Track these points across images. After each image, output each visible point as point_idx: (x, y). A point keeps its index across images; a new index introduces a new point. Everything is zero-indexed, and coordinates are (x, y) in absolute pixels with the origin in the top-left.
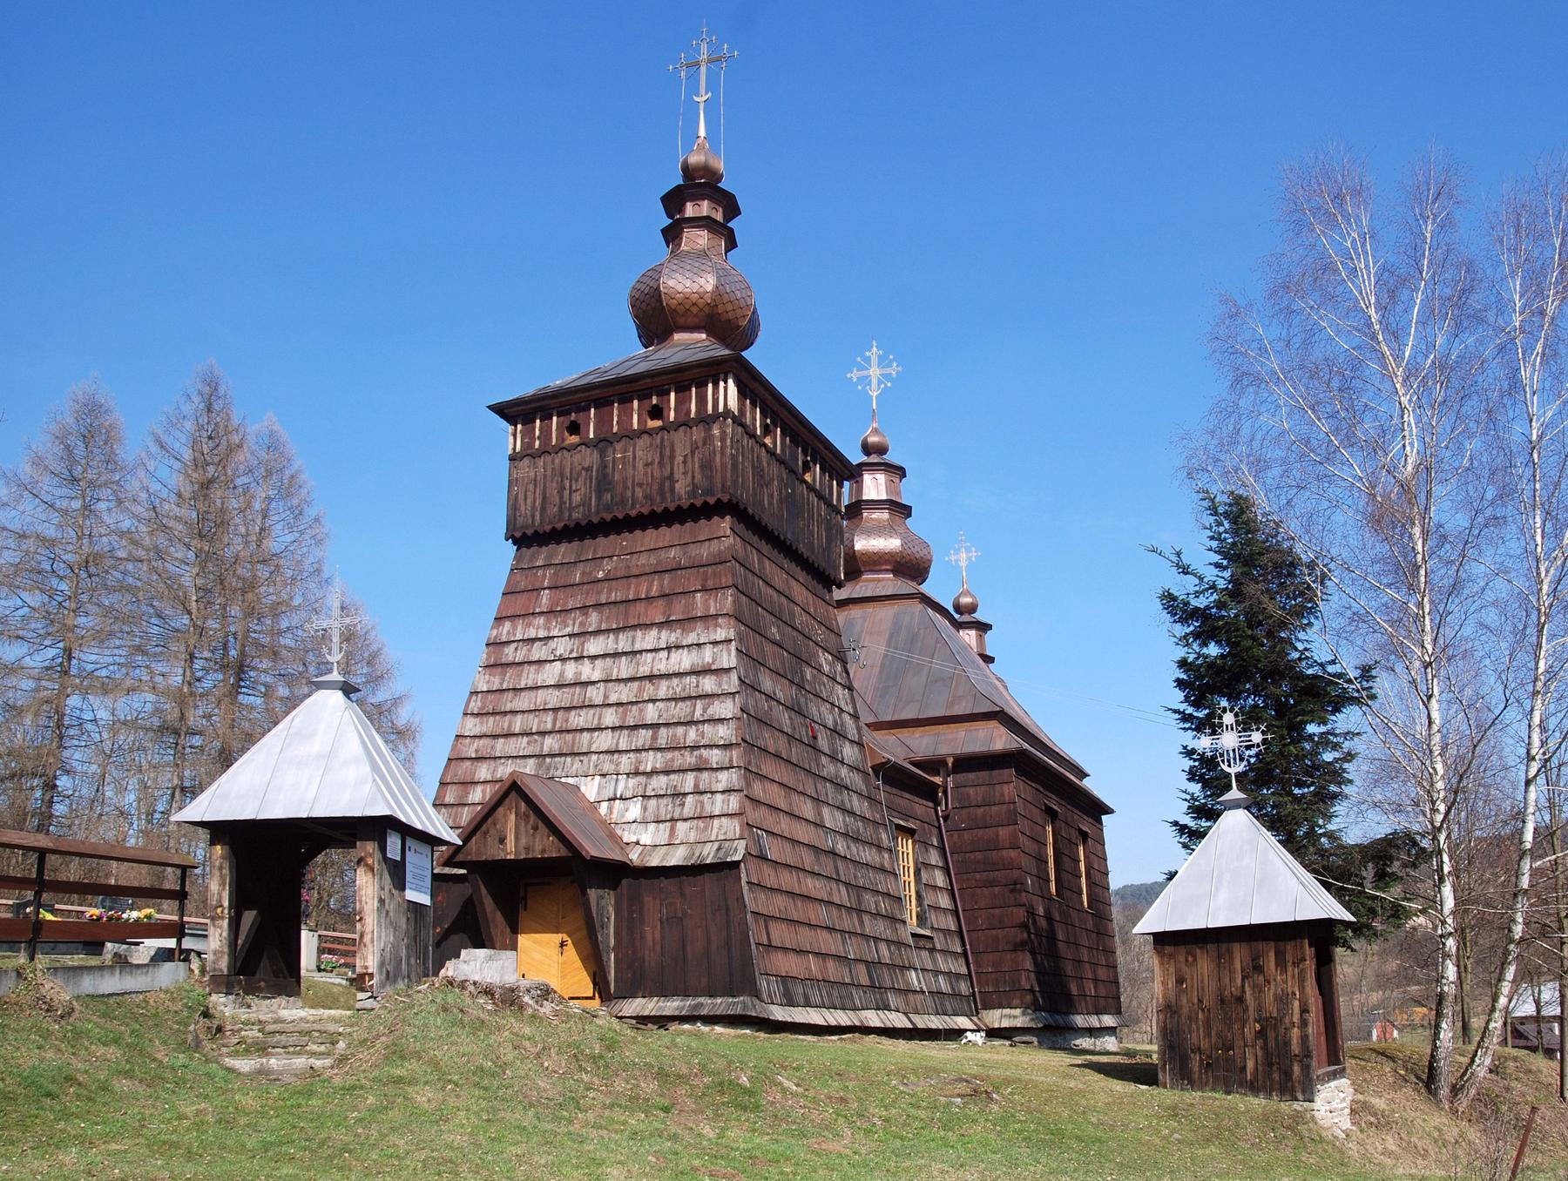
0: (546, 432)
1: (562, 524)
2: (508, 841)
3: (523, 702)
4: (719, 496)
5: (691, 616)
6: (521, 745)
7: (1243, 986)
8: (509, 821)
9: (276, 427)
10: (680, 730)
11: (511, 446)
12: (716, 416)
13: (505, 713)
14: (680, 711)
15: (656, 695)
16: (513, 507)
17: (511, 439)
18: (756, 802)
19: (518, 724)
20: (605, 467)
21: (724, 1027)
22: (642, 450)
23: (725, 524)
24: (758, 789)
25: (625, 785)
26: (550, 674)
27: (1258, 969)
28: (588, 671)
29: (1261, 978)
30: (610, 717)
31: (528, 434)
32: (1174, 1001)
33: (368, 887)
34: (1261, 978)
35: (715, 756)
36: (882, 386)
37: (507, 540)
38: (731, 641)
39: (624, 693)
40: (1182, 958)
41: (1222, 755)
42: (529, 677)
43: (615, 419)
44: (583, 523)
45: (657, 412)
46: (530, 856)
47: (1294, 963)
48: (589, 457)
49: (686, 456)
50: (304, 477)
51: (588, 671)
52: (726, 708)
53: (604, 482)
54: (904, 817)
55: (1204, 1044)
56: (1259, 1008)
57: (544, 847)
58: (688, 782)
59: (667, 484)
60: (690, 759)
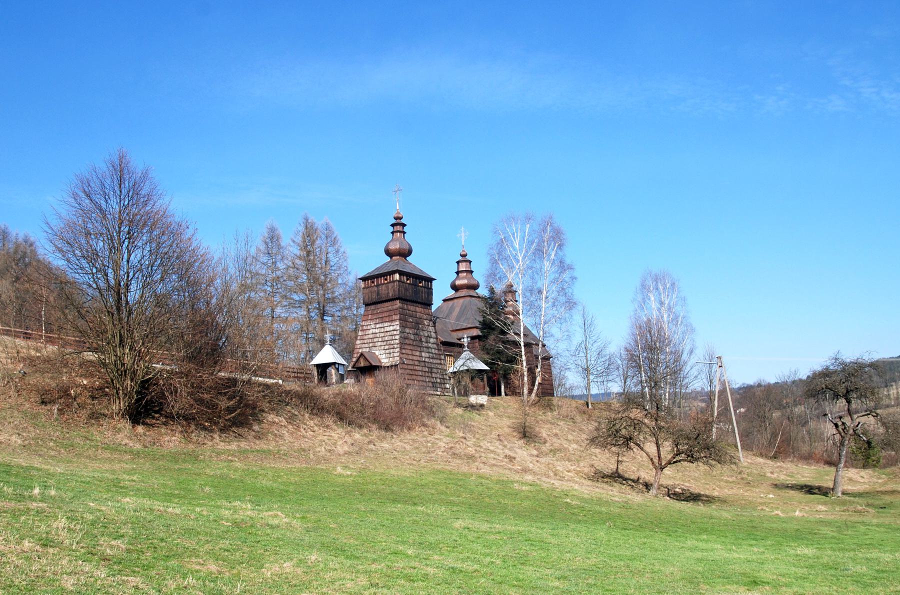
0: (368, 283)
3: (366, 337)
6: (367, 345)
8: (362, 360)
9: (328, 221)
12: (395, 281)
14: (390, 338)
18: (403, 354)
19: (366, 341)
22: (384, 287)
23: (398, 301)
24: (404, 351)
25: (383, 352)
26: (371, 332)
28: (377, 331)
30: (380, 340)
31: (365, 283)
33: (333, 371)
35: (396, 346)
39: (382, 335)
42: (368, 332)
45: (386, 280)
48: (376, 289)
50: (338, 237)
51: (377, 331)
52: (397, 337)
53: (378, 294)
57: (367, 364)
58: (392, 351)
60: (392, 347)
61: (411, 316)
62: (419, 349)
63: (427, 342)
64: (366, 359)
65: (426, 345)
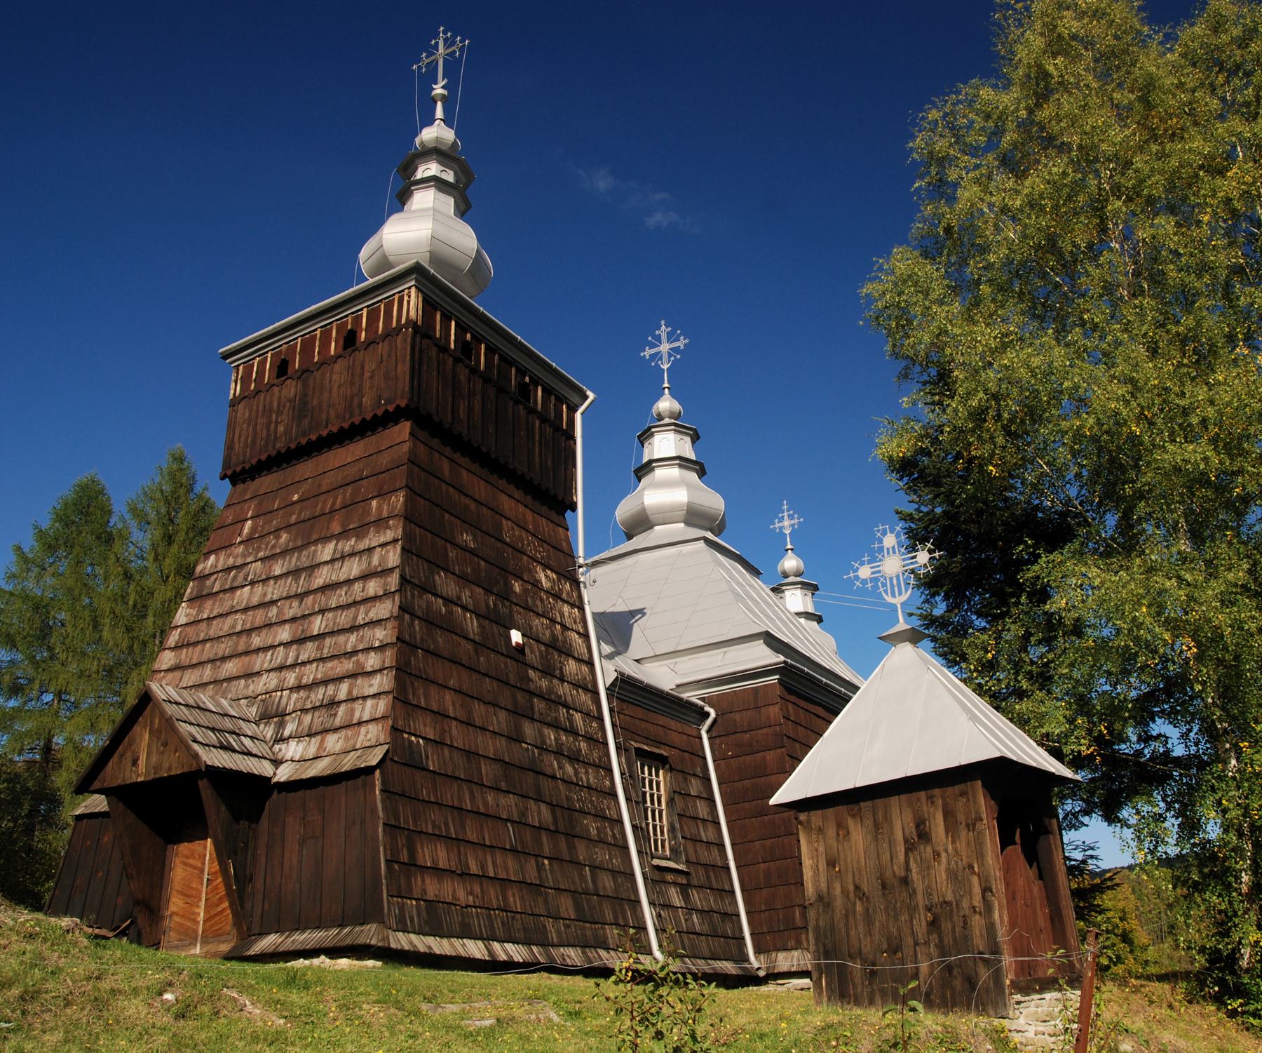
1: (266, 455)
2: (140, 762)
4: (398, 402)
5: (366, 522)
7: (907, 863)
8: (143, 738)
10: (341, 639)
11: (232, 392)
13: (196, 643)
14: (344, 619)
15: (327, 605)
16: (230, 447)
17: (233, 385)
20: (306, 395)
21: (357, 960)
26: (244, 596)
27: (923, 835)
29: (929, 849)
32: (825, 890)
34: (929, 849)
35: (372, 661)
36: (672, 359)
37: (223, 478)
38: (398, 540)
40: (831, 831)
41: (884, 585)
43: (317, 350)
44: (283, 451)
46: (157, 776)
47: (967, 825)
49: (373, 371)
52: (384, 609)
54: (655, 744)
55: (867, 947)
56: (928, 893)
59: (356, 400)
60: (348, 666)
61: (474, 526)
62: (505, 698)
63: (547, 672)
64: (167, 731)
65: (544, 683)
